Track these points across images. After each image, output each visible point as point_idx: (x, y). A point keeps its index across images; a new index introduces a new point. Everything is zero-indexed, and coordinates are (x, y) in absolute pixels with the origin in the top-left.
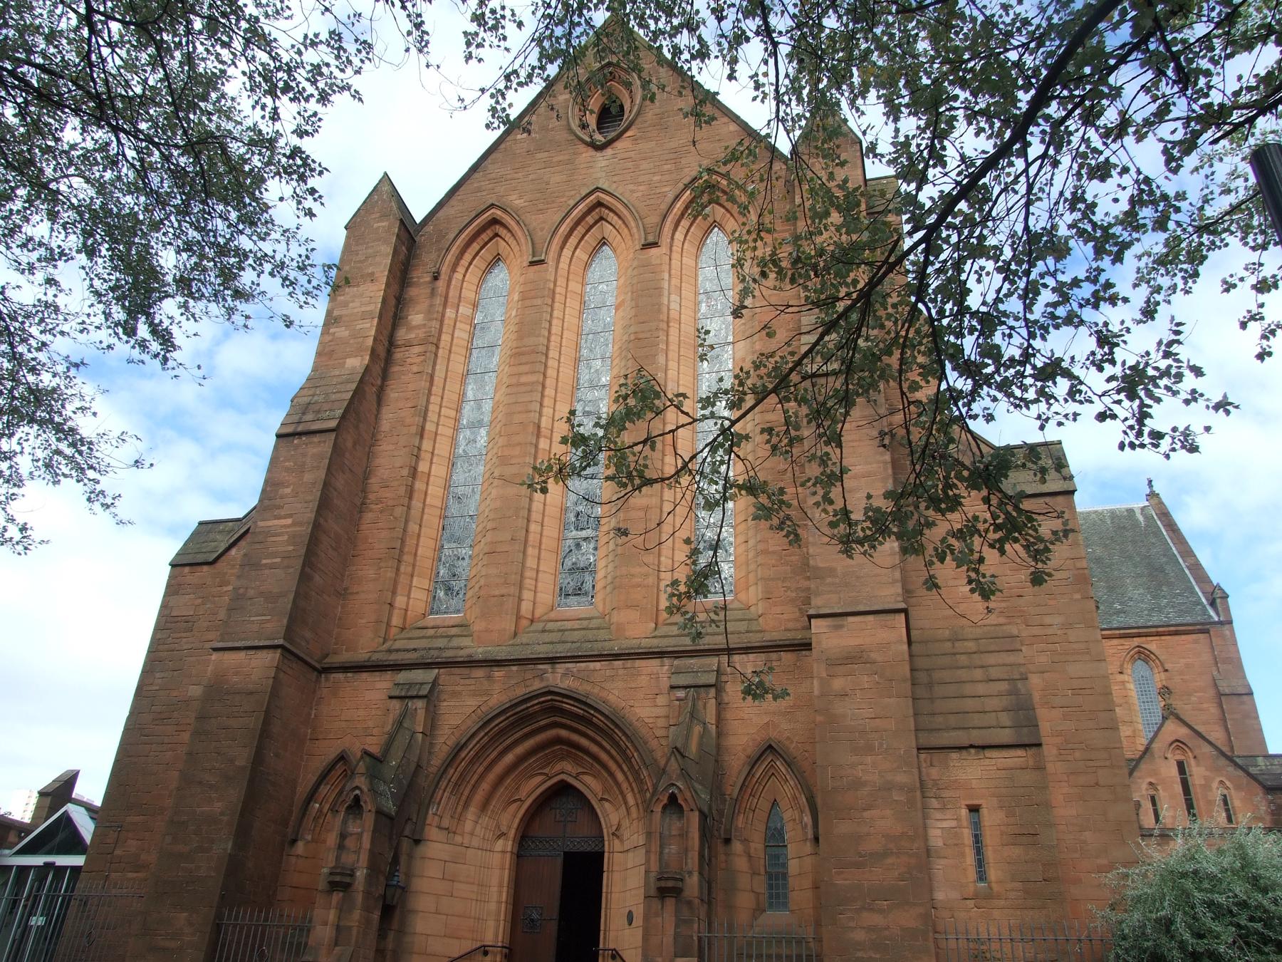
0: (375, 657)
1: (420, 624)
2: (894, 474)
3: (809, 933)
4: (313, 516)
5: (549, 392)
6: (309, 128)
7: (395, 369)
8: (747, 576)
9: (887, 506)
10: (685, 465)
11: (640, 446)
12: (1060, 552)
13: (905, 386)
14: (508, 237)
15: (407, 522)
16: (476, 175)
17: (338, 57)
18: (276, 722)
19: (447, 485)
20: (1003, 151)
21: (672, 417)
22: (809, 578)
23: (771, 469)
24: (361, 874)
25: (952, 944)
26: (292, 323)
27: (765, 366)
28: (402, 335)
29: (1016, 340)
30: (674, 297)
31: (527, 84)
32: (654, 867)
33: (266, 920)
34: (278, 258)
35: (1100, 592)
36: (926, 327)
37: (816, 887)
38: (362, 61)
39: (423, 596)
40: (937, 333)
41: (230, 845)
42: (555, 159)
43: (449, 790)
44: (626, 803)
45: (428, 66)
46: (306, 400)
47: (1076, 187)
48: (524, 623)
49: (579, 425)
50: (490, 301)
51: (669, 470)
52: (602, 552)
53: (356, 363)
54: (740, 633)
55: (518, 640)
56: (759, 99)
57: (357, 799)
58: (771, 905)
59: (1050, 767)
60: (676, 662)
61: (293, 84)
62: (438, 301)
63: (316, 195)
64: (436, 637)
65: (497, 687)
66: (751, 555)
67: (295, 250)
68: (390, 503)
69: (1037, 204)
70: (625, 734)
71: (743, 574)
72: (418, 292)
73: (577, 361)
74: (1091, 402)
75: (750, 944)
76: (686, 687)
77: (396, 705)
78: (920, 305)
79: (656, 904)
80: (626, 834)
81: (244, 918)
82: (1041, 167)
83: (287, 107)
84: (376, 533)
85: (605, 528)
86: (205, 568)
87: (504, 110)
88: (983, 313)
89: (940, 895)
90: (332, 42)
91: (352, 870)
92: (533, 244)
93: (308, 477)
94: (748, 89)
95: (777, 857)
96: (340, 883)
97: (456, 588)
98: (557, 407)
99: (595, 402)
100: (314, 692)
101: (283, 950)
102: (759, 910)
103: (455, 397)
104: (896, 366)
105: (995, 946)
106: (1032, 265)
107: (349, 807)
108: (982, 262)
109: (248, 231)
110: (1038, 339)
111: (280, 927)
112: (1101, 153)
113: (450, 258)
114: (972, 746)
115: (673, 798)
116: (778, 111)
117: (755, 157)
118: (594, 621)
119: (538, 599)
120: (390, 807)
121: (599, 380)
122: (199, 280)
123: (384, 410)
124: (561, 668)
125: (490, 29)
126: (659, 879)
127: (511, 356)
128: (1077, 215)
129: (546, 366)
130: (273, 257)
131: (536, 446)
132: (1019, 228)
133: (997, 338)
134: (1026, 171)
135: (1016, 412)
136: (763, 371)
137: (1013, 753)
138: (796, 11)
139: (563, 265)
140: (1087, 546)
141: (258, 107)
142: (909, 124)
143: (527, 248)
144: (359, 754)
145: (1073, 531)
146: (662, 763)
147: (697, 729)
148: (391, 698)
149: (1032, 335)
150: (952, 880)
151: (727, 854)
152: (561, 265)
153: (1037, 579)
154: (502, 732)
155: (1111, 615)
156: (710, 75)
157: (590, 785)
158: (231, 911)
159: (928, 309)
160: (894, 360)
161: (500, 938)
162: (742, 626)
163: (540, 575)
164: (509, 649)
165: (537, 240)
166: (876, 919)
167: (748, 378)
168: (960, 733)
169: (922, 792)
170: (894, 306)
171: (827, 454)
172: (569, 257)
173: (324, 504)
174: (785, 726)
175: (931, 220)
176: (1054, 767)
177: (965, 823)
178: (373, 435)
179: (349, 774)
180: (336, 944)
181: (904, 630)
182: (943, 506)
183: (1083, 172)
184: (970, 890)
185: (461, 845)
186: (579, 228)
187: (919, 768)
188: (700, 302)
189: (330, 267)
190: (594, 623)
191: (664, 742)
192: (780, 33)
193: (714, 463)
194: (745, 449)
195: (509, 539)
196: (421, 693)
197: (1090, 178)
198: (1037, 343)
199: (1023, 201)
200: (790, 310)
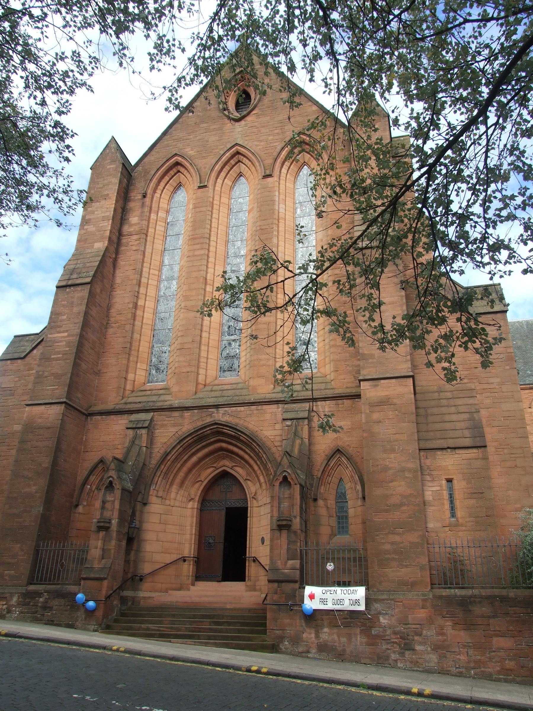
0: (117, 407)
1: (142, 388)
2: (407, 302)
3: (360, 546)
4: (79, 331)
5: (211, 260)
6: (64, 110)
7: (123, 248)
8: (324, 359)
9: (403, 322)
10: (290, 300)
11: (265, 289)
12: (497, 349)
13: (415, 254)
14: (185, 172)
15: (132, 333)
16: (166, 137)
17: (78, 66)
18: (63, 446)
19: (155, 312)
20: (472, 122)
21: (282, 273)
22: (359, 360)
23: (340, 302)
24: (115, 522)
25: (437, 550)
26: (61, 224)
27: (336, 246)
28: (126, 229)
29: (478, 229)
30: (282, 206)
31: (190, 85)
32: (276, 514)
33: (64, 546)
34: (51, 187)
35: (520, 365)
36: (427, 222)
37: (364, 523)
38: (93, 68)
39: (143, 373)
40: (433, 225)
41: (42, 509)
42: (212, 127)
43: (162, 477)
44: (259, 481)
45: (134, 72)
46: (72, 267)
47: (513, 142)
48: (201, 387)
49: (229, 279)
50: (175, 209)
51: (281, 302)
52: (243, 347)
53: (100, 246)
54: (321, 390)
55: (197, 396)
56: (327, 93)
57: (111, 483)
58: (339, 533)
59: (491, 458)
60: (286, 406)
61: (54, 84)
62: (146, 209)
63: (70, 149)
64: (152, 395)
65: (186, 421)
66: (327, 347)
67: (62, 182)
68: (123, 323)
69: (492, 151)
70: (258, 445)
71: (323, 358)
72: (134, 205)
73: (227, 242)
74: (521, 262)
75: (328, 553)
76: (291, 419)
77: (131, 433)
78: (424, 210)
79: (277, 533)
80: (260, 497)
81: (51, 546)
82: (495, 130)
83: (50, 97)
84: (115, 339)
85: (245, 335)
86: (19, 361)
87: (176, 99)
88: (460, 214)
89: (430, 525)
90: (75, 58)
91: (110, 520)
92: (200, 176)
93: (75, 310)
94: (322, 84)
95: (343, 507)
96: (104, 527)
97: (162, 369)
98: (216, 268)
99: (238, 265)
100: (84, 427)
101: (74, 562)
102: (333, 535)
103: (158, 264)
104: (410, 243)
105: (460, 550)
106: (488, 186)
107: (107, 487)
108: (459, 184)
109: (34, 171)
110: (491, 228)
111: (72, 550)
112: (529, 122)
113: (152, 185)
114: (449, 448)
115: (285, 478)
116: (338, 100)
117: (325, 126)
119: (208, 374)
120: (129, 486)
121: (240, 252)
122: (7, 200)
123: (117, 272)
124: (222, 410)
125: (165, 54)
126: (278, 521)
127: (189, 240)
128: (513, 158)
129: (209, 245)
130: (49, 186)
131: (205, 290)
132: (481, 166)
133: (467, 228)
134: (486, 132)
135: (477, 270)
136: (335, 249)
137: (470, 451)
138: (349, 41)
139: (218, 188)
140: (513, 340)
141: (32, 98)
142: (419, 106)
143: (196, 179)
144: (111, 459)
145: (504, 339)
146: (279, 459)
147: (298, 442)
148: (127, 428)
149: (487, 226)
150: (437, 518)
151: (315, 507)
152: (217, 188)
153: (485, 365)
154: (190, 446)
155: (525, 377)
156: (300, 78)
157: (240, 472)
158: (44, 543)
159: (429, 212)
160: (409, 241)
162: (323, 386)
163: (209, 360)
164: (192, 401)
165: (202, 174)
166: (397, 538)
167: (326, 252)
168: (442, 441)
169: (422, 472)
170: (409, 210)
171: (371, 294)
172: (222, 183)
173: (85, 325)
174: (346, 439)
175: (431, 161)
176: (493, 457)
177: (444, 488)
178: (112, 286)
179: (106, 469)
180: (103, 558)
181: (412, 387)
182: (436, 322)
183: (518, 133)
184: (447, 521)
185: (169, 505)
186: (226, 167)
187: (420, 460)
188: (296, 208)
189: (81, 191)
190: (240, 386)
191: (280, 449)
192: (340, 54)
193: (307, 299)
194: (324, 291)
195: (191, 345)
196: (144, 426)
197: (522, 136)
198: (490, 231)
199: (484, 150)
200: (350, 212)
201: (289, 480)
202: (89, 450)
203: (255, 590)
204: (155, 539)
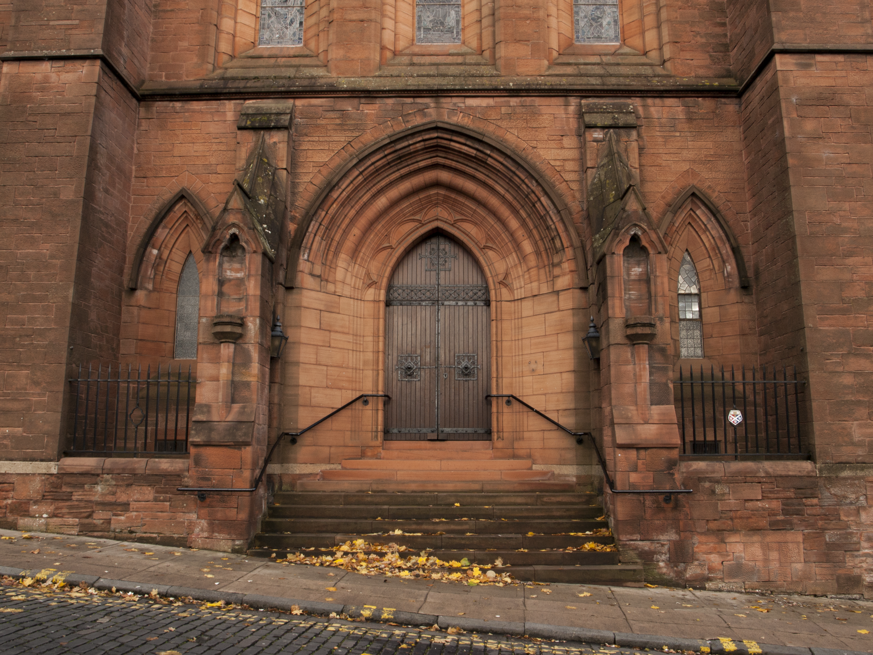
1: (251, 52)
39: (249, 21)
43: (320, 234)
57: (234, 238)
77: (249, 140)
91: (242, 319)
96: (227, 331)
107: (226, 248)
115: (635, 239)
118: (468, 57)
124: (448, 103)
161: (380, 387)
180: (233, 401)
201: (644, 243)
202: (149, 174)
203: (515, 457)
204: (313, 361)
